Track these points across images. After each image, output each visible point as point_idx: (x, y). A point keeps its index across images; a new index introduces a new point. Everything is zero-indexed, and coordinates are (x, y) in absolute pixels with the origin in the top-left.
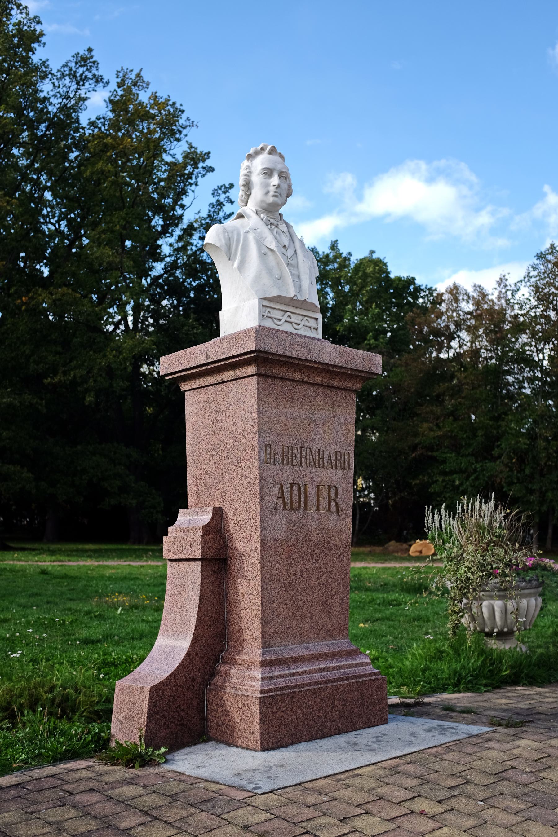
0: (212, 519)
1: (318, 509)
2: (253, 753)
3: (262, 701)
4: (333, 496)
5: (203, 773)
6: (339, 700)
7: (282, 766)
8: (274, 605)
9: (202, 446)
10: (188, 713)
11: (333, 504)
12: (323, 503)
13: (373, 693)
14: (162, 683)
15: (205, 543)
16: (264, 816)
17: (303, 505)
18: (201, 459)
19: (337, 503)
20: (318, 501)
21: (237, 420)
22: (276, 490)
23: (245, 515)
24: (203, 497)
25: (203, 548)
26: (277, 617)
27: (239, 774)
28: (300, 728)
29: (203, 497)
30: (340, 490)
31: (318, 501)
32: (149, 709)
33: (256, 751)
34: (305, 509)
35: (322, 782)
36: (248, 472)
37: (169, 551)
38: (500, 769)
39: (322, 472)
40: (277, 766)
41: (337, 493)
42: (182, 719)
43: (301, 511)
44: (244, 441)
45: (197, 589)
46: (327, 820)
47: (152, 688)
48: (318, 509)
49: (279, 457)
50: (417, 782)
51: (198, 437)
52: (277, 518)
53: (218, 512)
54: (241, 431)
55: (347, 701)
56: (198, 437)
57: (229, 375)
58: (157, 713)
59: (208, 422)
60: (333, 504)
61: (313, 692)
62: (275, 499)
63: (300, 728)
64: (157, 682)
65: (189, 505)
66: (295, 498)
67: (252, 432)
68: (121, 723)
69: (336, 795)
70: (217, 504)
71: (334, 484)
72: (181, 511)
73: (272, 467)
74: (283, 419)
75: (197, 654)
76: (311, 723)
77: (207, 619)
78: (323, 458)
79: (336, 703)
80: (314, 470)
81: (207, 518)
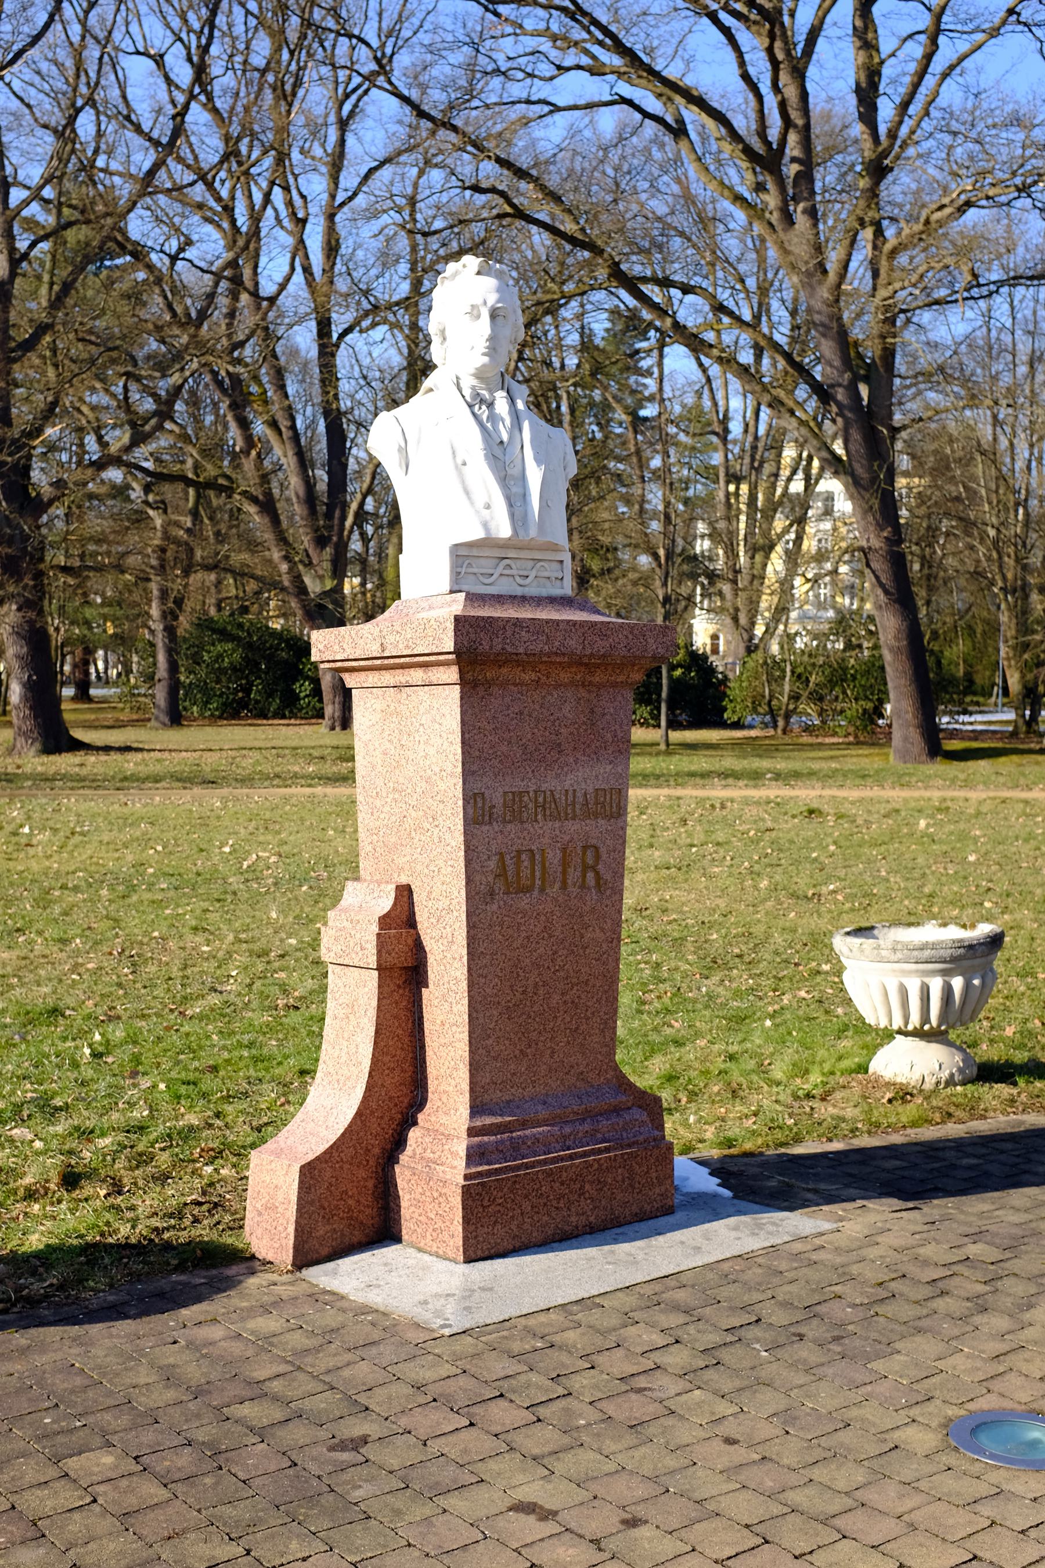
0: (395, 904)
1: (564, 885)
2: (452, 1266)
3: (466, 1191)
4: (590, 861)
5: (375, 1299)
6: (591, 1183)
7: (491, 1289)
8: (490, 1042)
9: (380, 782)
10: (354, 1204)
11: (590, 875)
12: (574, 875)
13: (649, 1169)
14: (318, 1158)
15: (382, 942)
16: (447, 1370)
17: (538, 882)
18: (378, 803)
19: (597, 873)
20: (564, 873)
21: (432, 751)
22: (492, 864)
23: (444, 903)
24: (382, 865)
25: (379, 952)
26: (495, 1059)
27: (426, 1302)
28: (526, 1226)
29: (382, 865)
30: (603, 850)
31: (564, 873)
32: (299, 1198)
33: (455, 1261)
34: (542, 890)
35: (543, 1318)
36: (448, 836)
37: (329, 950)
38: (817, 1298)
39: (573, 827)
40: (483, 1289)
41: (597, 857)
42: (350, 1210)
43: (536, 893)
44: (442, 786)
45: (372, 1013)
46: (534, 1377)
47: (302, 1167)
48: (564, 885)
49: (498, 811)
50: (682, 1319)
51: (374, 767)
52: (495, 907)
53: (405, 893)
54: (437, 769)
55: (605, 1183)
56: (374, 767)
57: (417, 675)
58: (312, 1203)
59: (388, 745)
60: (590, 875)
61: (550, 1173)
62: (491, 879)
63: (526, 1226)
64: (311, 1157)
65: (450, 626)
66: (526, 873)
67: (452, 775)
68: (260, 1214)
69: (556, 1339)
70: (404, 880)
71: (594, 842)
72: (350, 886)
73: (485, 828)
74: (504, 748)
75: (372, 1113)
76: (546, 1218)
77: (386, 1059)
78: (574, 804)
79: (587, 1187)
80: (557, 824)
81: (386, 903)
